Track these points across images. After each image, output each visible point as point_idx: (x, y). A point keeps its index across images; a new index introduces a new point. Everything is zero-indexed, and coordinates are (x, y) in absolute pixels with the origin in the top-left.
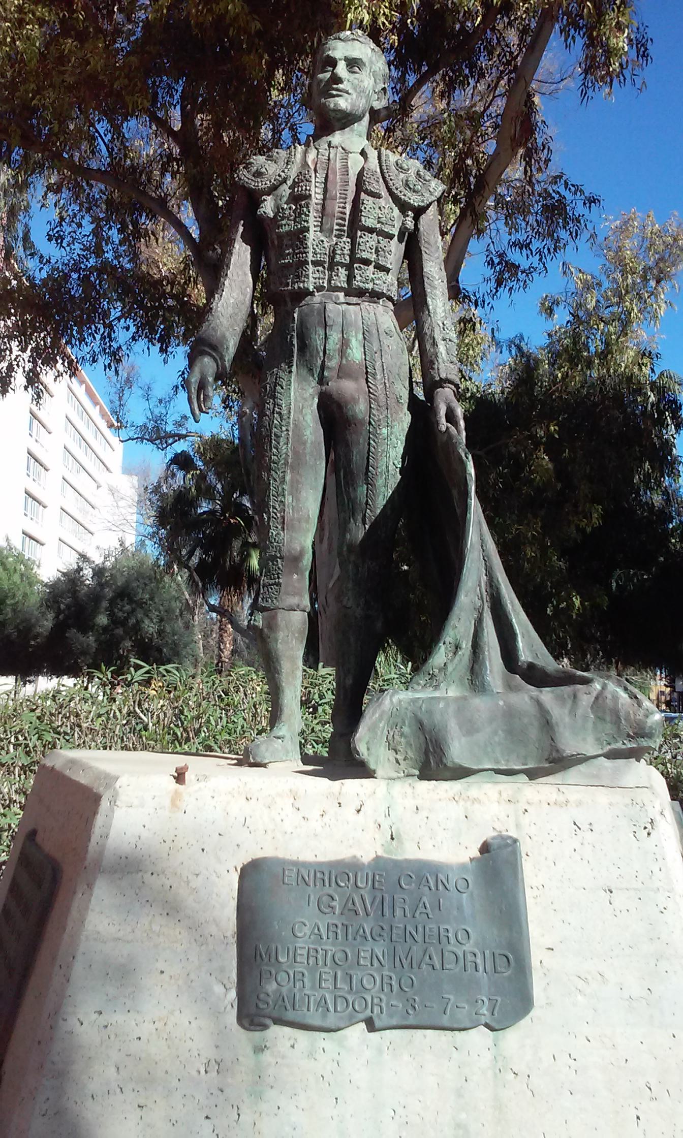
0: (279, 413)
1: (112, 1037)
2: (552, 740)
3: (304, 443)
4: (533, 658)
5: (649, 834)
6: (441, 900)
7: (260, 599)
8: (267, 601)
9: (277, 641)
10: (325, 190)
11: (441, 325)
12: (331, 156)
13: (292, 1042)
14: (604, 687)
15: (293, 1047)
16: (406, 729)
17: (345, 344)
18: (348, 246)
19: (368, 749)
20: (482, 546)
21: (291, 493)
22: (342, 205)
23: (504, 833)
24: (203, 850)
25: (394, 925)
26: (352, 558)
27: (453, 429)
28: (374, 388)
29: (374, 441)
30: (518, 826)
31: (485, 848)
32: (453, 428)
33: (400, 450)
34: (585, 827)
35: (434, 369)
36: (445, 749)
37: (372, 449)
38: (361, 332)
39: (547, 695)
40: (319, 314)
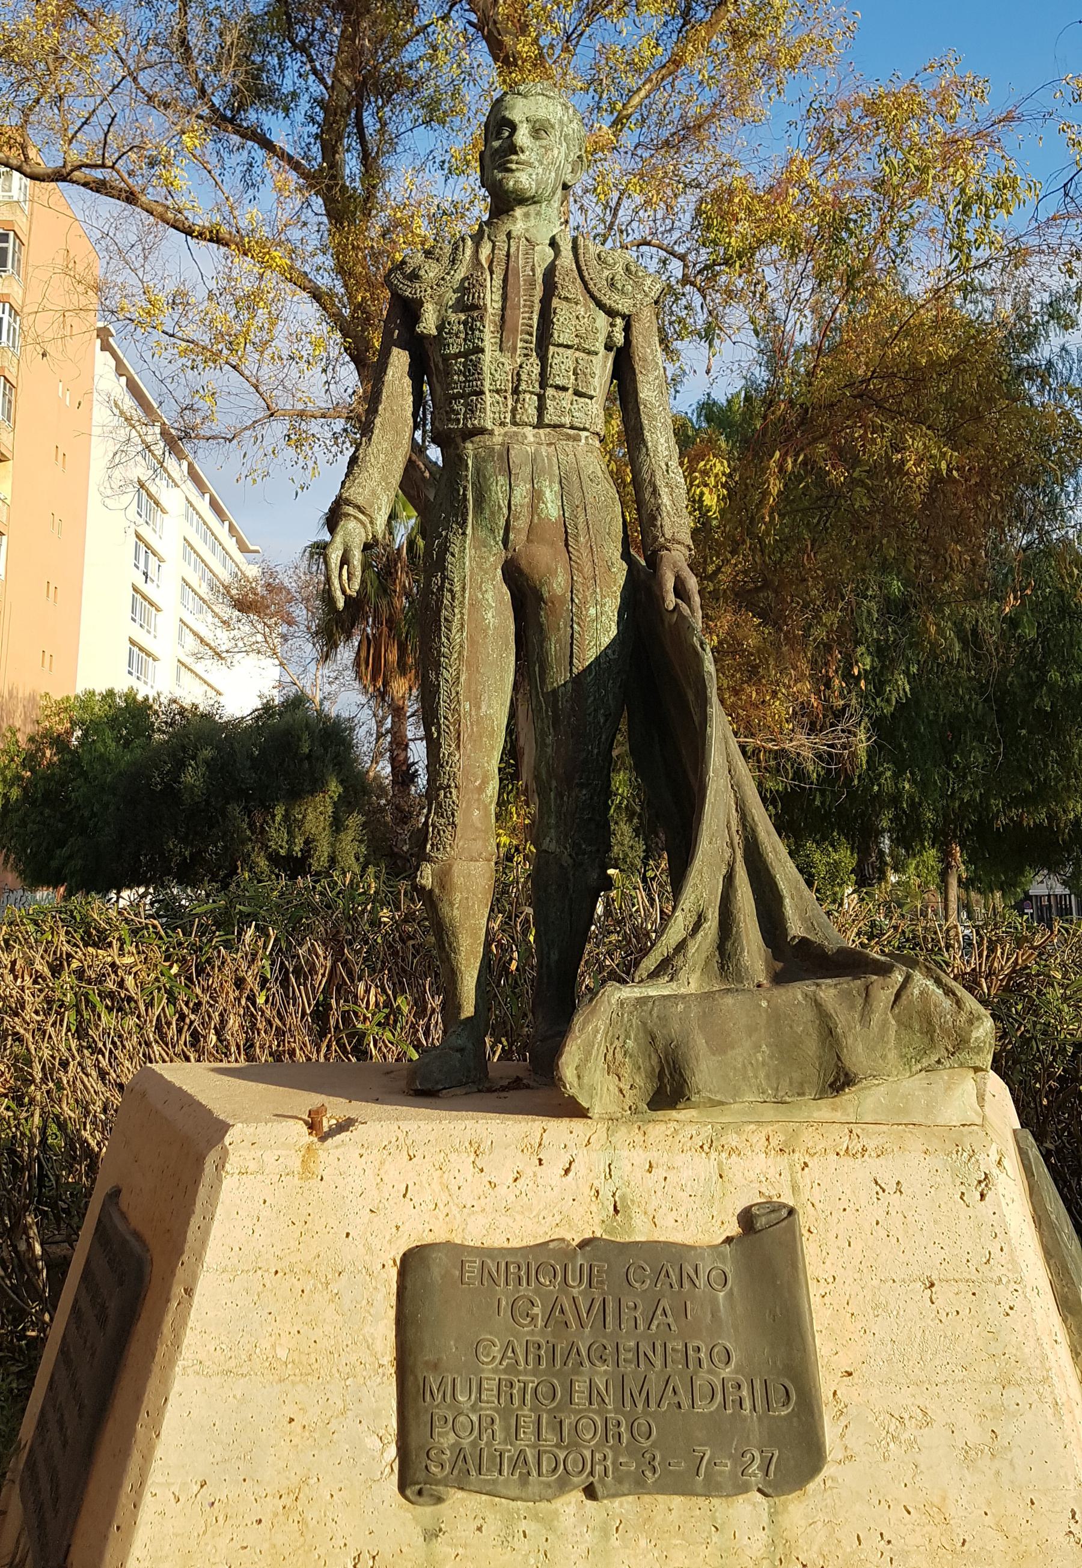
0: (451, 591)
1: (221, 1519)
2: (839, 1058)
3: (485, 631)
4: (807, 929)
5: (982, 1196)
6: (688, 1303)
7: (429, 846)
8: (438, 849)
9: (451, 905)
10: (505, 297)
11: (664, 467)
12: (512, 250)
13: (479, 1522)
14: (908, 978)
15: (479, 1529)
16: (630, 1043)
17: (536, 496)
18: (537, 370)
19: (579, 1077)
20: (730, 771)
21: (467, 699)
22: (527, 315)
23: (775, 1199)
24: (348, 1235)
25: (621, 1341)
26: (554, 784)
27: (683, 606)
28: (576, 553)
29: (579, 624)
30: (795, 1189)
31: (747, 1218)
32: (684, 605)
33: (622, 583)
34: (891, 1187)
35: (655, 526)
36: (687, 1074)
37: (576, 635)
38: (557, 479)
39: (828, 991)
40: (500, 456)
